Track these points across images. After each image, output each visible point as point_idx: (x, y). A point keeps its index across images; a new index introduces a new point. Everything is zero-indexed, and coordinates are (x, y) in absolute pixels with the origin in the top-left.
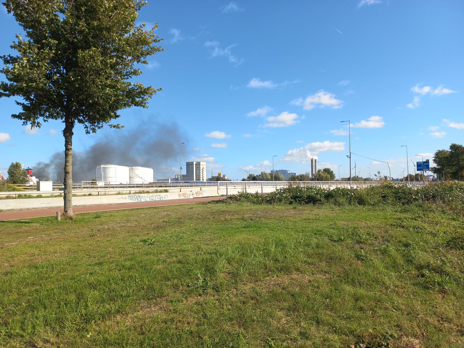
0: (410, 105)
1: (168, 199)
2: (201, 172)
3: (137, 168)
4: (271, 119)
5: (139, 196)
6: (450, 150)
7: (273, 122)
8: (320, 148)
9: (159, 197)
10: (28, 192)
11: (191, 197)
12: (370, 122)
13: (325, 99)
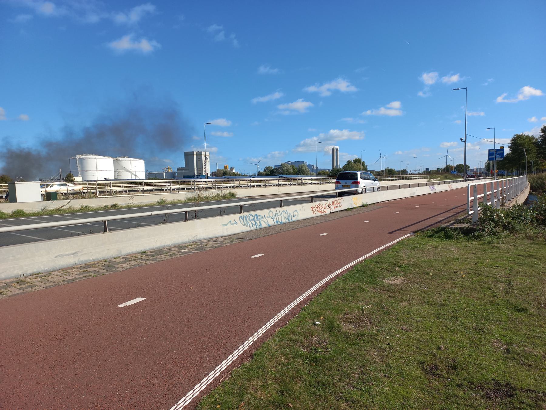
0: (420, 94)
3: (121, 159)
4: (281, 107)
5: (256, 215)
6: (542, 134)
9: (286, 216)
11: (328, 212)
13: (343, 85)
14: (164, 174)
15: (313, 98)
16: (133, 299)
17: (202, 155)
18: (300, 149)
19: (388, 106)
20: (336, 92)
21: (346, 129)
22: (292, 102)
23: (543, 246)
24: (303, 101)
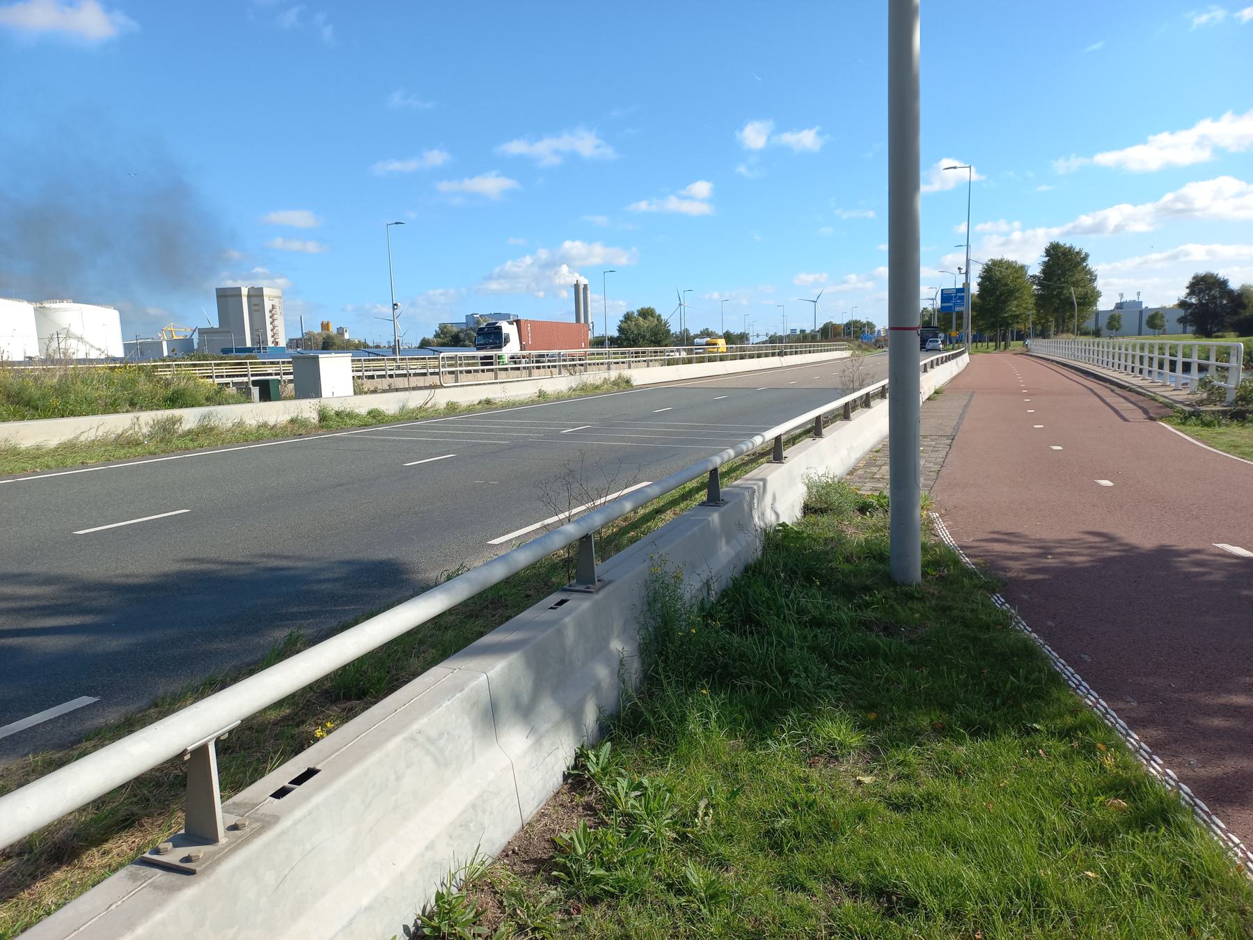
0: (742, 169)
2: (268, 320)
3: (53, 306)
4: (444, 186)
10: (1088, 551)
13: (586, 144)
14: (165, 344)
15: (518, 168)
16: (66, 700)
17: (262, 296)
18: (494, 286)
19: (683, 193)
20: (573, 158)
22: (471, 177)
23: (882, 642)
24: (498, 176)
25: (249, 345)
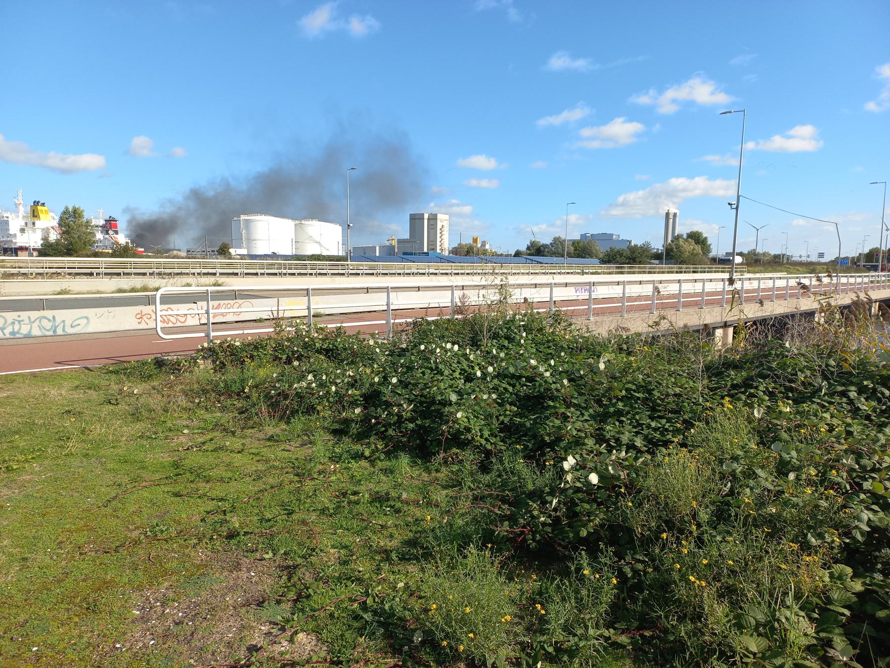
0: (871, 106)
1: (91, 329)
3: (307, 222)
4: (586, 132)
7: (593, 138)
8: (684, 190)
9: (45, 323)
12: (791, 141)
13: (703, 92)
18: (614, 212)
19: (792, 132)
20: (689, 104)
21: (699, 176)
25: (425, 250)
